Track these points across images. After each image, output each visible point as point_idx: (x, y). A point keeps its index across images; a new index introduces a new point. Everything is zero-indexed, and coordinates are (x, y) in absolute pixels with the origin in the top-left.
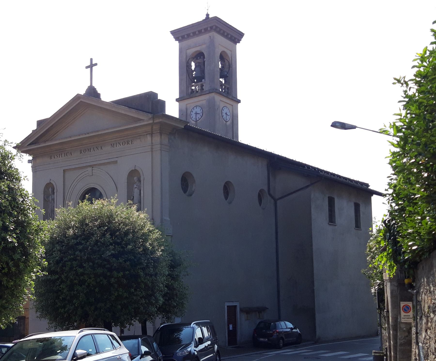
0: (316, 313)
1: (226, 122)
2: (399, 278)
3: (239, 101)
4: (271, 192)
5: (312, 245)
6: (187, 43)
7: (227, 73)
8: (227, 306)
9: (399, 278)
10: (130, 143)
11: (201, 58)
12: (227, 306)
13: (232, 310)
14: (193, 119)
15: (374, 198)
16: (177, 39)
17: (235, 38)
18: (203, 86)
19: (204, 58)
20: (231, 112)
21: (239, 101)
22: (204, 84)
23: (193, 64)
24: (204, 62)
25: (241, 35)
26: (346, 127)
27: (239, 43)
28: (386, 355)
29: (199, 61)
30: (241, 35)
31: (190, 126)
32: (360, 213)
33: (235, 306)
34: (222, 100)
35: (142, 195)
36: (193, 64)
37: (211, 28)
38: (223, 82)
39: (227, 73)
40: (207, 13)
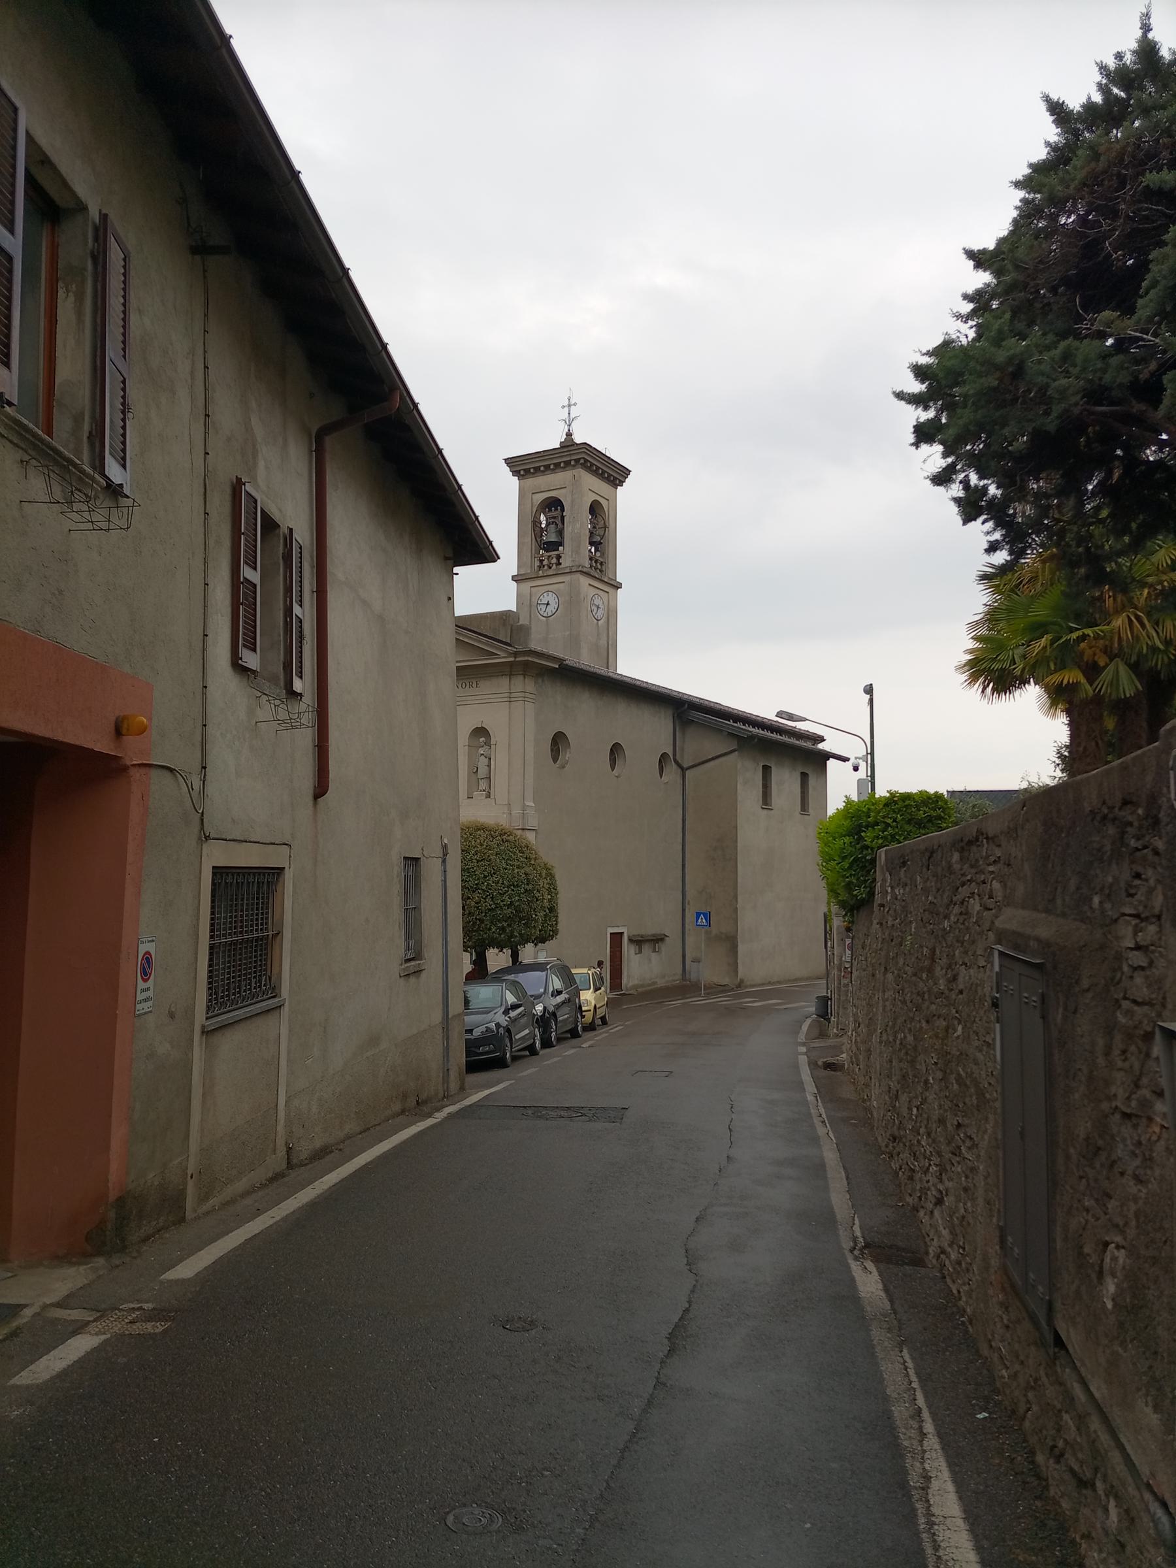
0: (739, 944)
1: (598, 620)
2: (1144, 560)
3: (618, 586)
4: (678, 758)
5: (736, 841)
6: (531, 482)
7: (602, 539)
8: (611, 934)
9: (1144, 560)
10: (475, 685)
11: (556, 509)
12: (611, 934)
13: (616, 938)
14: (542, 613)
15: (832, 764)
16: (516, 473)
17: (615, 478)
18: (561, 557)
19: (563, 510)
20: (606, 603)
21: (618, 586)
22: (563, 555)
23: (543, 518)
24: (563, 518)
25: (625, 472)
26: (792, 718)
27: (622, 486)
28: (831, 999)
29: (554, 514)
30: (625, 472)
31: (567, 665)
32: (808, 788)
33: (622, 933)
34: (591, 583)
35: (492, 767)
36: (543, 518)
37: (577, 461)
38: (987, 1415)
39: (602, 539)
40: (569, 434)
